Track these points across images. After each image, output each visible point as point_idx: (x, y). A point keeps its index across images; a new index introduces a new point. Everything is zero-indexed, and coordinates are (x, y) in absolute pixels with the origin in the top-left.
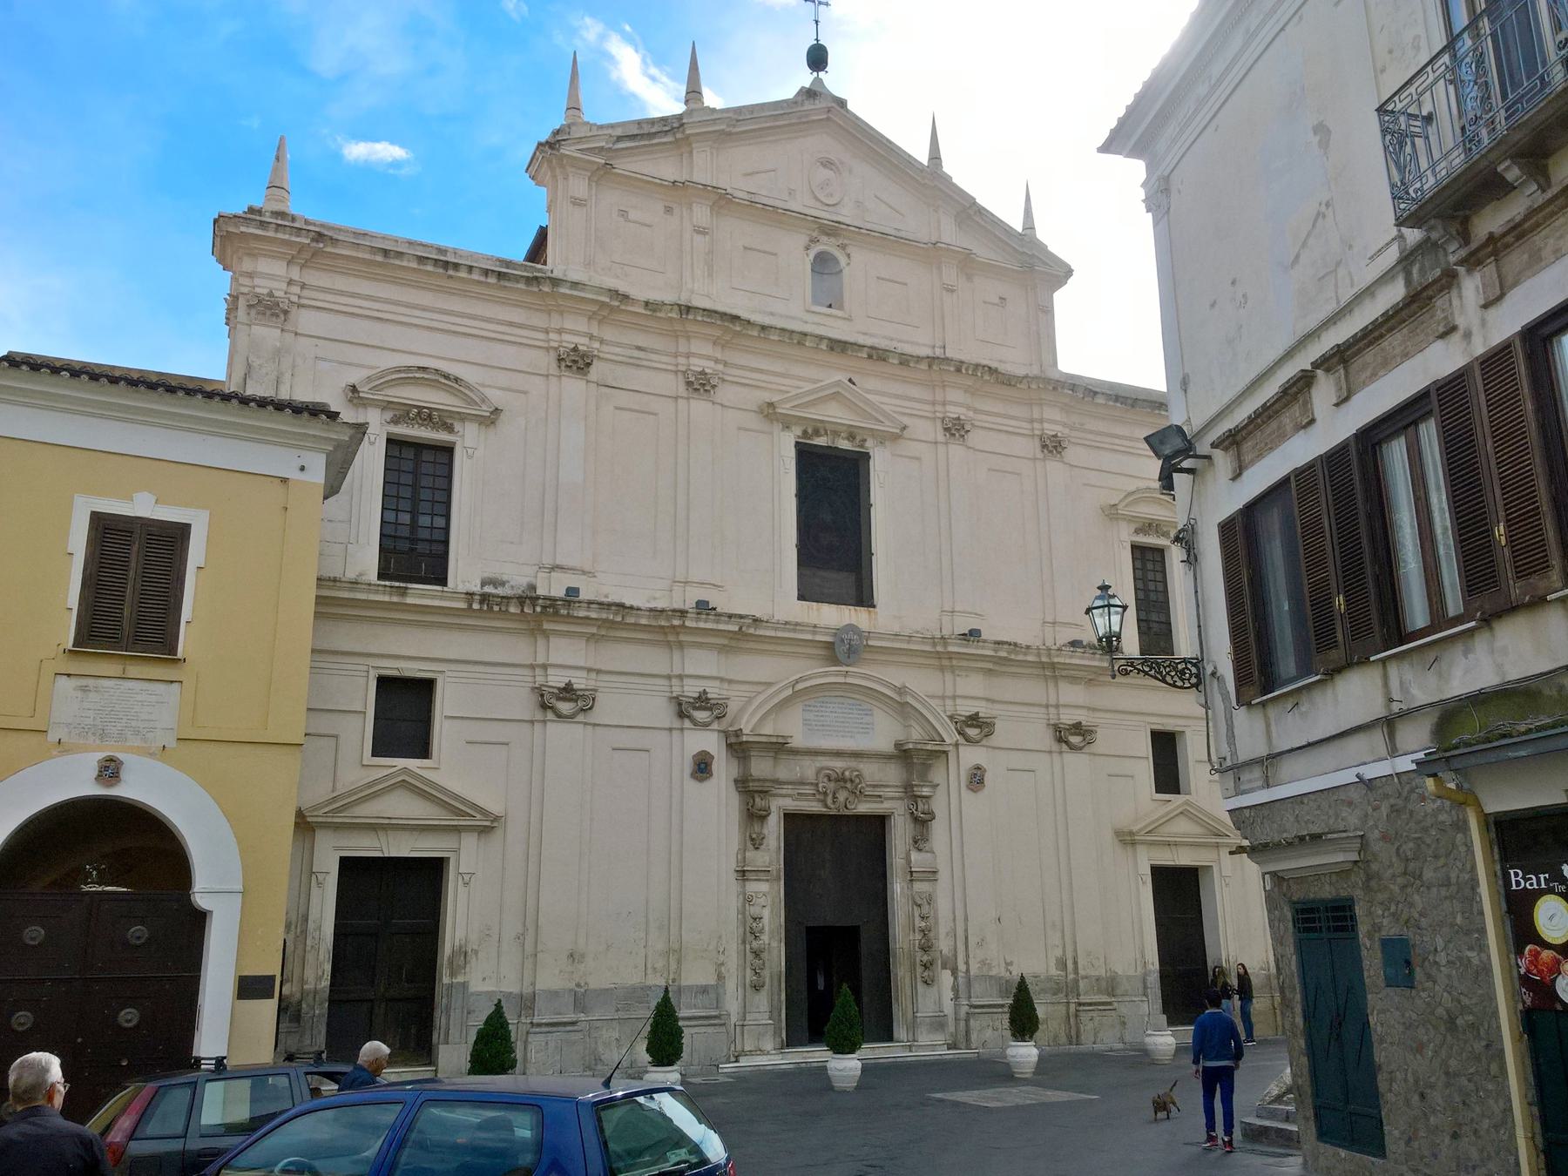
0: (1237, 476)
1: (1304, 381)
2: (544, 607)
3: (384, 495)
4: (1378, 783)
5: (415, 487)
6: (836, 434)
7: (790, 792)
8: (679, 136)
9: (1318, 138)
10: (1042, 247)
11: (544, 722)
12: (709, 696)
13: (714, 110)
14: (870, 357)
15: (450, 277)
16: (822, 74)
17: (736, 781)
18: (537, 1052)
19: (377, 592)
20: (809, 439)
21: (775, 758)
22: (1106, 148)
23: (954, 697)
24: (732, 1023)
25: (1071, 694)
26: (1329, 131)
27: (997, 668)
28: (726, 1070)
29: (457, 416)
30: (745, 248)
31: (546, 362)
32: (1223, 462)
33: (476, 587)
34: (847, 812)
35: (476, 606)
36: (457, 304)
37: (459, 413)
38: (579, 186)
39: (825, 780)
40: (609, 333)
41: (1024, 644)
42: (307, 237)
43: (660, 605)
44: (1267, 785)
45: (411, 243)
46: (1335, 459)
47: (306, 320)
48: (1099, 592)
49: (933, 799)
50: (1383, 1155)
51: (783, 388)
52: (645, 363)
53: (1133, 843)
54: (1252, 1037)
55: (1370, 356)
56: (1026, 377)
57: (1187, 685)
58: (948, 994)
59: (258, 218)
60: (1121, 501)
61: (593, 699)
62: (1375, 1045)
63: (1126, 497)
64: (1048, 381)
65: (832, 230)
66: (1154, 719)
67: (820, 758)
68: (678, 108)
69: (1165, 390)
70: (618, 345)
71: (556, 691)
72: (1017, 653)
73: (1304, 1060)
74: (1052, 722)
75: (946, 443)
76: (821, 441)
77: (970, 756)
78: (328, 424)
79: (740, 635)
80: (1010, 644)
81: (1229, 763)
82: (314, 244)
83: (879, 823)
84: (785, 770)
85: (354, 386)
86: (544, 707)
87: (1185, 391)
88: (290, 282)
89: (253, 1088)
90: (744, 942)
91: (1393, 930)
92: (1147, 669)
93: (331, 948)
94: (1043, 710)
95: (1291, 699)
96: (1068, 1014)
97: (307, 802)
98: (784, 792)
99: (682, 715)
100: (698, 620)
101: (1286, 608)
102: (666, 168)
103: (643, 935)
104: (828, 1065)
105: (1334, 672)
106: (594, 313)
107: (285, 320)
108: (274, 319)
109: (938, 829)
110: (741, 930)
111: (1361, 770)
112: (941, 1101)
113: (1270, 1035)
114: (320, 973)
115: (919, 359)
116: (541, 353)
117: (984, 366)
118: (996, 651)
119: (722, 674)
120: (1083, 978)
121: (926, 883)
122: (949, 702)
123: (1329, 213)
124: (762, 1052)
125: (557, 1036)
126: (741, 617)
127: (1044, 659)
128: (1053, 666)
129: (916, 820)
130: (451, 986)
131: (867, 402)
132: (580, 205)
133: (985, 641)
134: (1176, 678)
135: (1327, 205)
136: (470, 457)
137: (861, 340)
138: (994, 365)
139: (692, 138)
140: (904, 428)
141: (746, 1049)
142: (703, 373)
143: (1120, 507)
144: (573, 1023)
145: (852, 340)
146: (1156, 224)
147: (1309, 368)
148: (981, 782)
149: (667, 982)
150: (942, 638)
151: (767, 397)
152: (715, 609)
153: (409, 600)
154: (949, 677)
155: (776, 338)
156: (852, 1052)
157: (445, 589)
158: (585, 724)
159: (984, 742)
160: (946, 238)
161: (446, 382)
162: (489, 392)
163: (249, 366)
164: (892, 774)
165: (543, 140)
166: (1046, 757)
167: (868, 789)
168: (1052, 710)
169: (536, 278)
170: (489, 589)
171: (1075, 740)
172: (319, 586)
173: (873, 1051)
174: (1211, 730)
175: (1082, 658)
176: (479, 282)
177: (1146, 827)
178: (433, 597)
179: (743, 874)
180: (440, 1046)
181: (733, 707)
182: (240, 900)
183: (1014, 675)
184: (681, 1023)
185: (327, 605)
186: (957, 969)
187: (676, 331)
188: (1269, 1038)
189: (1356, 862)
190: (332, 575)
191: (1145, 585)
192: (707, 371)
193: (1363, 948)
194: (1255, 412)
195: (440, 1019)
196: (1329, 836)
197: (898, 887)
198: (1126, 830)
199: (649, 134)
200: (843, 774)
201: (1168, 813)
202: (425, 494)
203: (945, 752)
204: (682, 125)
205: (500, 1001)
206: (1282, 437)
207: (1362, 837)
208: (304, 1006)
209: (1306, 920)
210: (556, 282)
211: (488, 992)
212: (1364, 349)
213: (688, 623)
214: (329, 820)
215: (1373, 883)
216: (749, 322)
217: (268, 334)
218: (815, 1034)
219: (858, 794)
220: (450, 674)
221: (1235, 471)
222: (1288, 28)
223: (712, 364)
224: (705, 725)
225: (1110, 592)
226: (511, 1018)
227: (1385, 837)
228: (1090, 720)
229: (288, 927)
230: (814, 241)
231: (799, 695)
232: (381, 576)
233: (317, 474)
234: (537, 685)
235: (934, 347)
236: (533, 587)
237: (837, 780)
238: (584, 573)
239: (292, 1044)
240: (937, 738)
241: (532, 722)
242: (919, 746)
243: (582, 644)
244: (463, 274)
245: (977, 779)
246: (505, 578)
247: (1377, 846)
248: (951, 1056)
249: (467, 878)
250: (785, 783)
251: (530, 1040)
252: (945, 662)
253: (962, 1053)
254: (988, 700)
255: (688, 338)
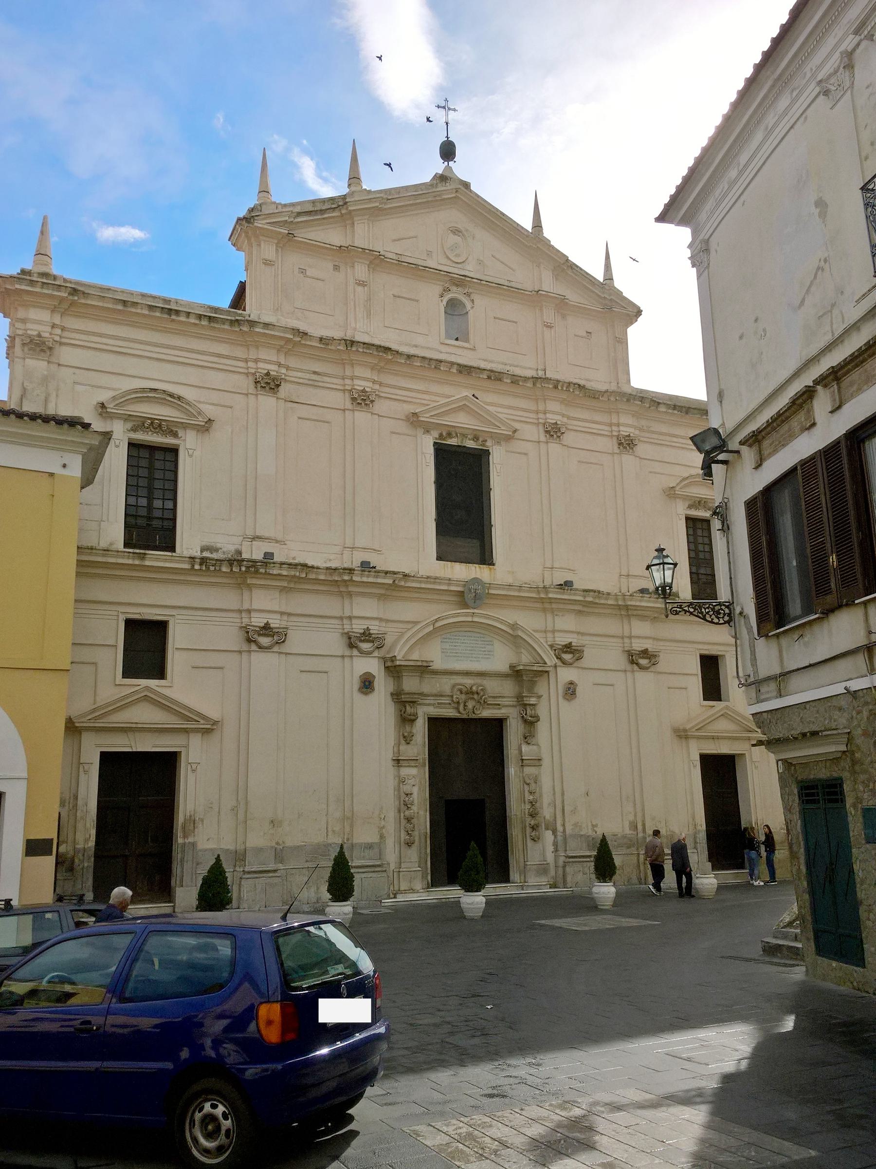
0: (758, 466)
1: (808, 394)
2: (248, 567)
3: (127, 485)
4: (860, 693)
5: (151, 479)
6: (464, 436)
7: (432, 702)
8: (343, 212)
9: (818, 210)
10: (619, 293)
11: (249, 652)
12: (371, 632)
13: (369, 192)
14: (489, 378)
15: (173, 320)
16: (451, 163)
17: (392, 694)
18: (247, 892)
19: (123, 557)
20: (444, 440)
21: (421, 677)
22: (662, 218)
23: (554, 631)
24: (391, 870)
25: (640, 628)
26: (826, 205)
27: (585, 609)
28: (386, 904)
29: (180, 425)
30: (394, 296)
31: (247, 384)
32: (748, 454)
33: (197, 553)
34: (474, 716)
35: (197, 567)
36: (178, 341)
37: (182, 423)
38: (268, 250)
39: (458, 693)
40: (293, 362)
41: (605, 591)
42: (65, 292)
43: (333, 565)
44: (780, 695)
45: (143, 295)
46: (830, 452)
47: (66, 355)
48: (656, 553)
49: (537, 707)
50: (864, 967)
51: (423, 402)
52: (320, 384)
53: (687, 738)
54: (775, 878)
55: (856, 375)
56: (607, 391)
57: (722, 621)
58: (550, 848)
59: (28, 278)
60: (678, 484)
61: (285, 635)
62: (858, 885)
63: (681, 481)
64: (623, 394)
65: (461, 281)
66: (700, 646)
67: (454, 677)
68: (344, 190)
69: (706, 399)
70: (301, 370)
71: (258, 629)
72: (599, 598)
73: (806, 897)
74: (626, 649)
75: (547, 443)
76: (453, 442)
77: (566, 675)
78: (82, 432)
79: (394, 586)
80: (595, 592)
81: (752, 679)
82: (71, 297)
83: (499, 724)
84: (429, 686)
85: (103, 404)
86: (249, 641)
87: (721, 402)
88: (54, 326)
89: (34, 921)
90: (399, 811)
91: (871, 801)
92: (692, 610)
93: (95, 818)
94: (620, 640)
95: (797, 632)
96: (639, 863)
97: (74, 713)
98: (427, 702)
99: (351, 646)
100: (362, 575)
101: (795, 564)
102: (335, 237)
103: (325, 806)
104: (461, 900)
105: (828, 612)
106: (282, 347)
107: (50, 355)
108: (42, 354)
109: (542, 728)
110: (397, 803)
111: (848, 684)
112: (542, 926)
113: (788, 876)
114: (88, 836)
115: (526, 379)
116: (242, 377)
117: (575, 384)
118: (585, 597)
119: (381, 616)
120: (248, 390)
121: (533, 768)
122: (550, 635)
123: (827, 267)
124: (412, 891)
125: (262, 881)
126: (394, 573)
127: (620, 603)
128: (627, 608)
129: (525, 721)
130: (184, 844)
131: (487, 412)
132: (268, 264)
133: (577, 590)
134: (713, 616)
135: (825, 261)
136: (191, 456)
137: (483, 365)
138: (582, 383)
139: (353, 213)
140: (515, 431)
141: (402, 888)
142: (364, 391)
143: (677, 489)
144: (275, 871)
145: (475, 365)
146: (699, 276)
147: (811, 384)
148: (574, 693)
149: (343, 841)
150: (544, 587)
151: (412, 408)
152: (375, 568)
153: (147, 563)
154: (549, 617)
155: (419, 364)
156: (478, 890)
157: (174, 554)
158: (280, 653)
159: (576, 664)
160: (546, 287)
161: (172, 400)
162: (201, 406)
163: (24, 390)
164: (508, 688)
165: (241, 216)
166: (622, 674)
167: (489, 699)
168: (627, 640)
169: (237, 320)
170: (206, 554)
171: (643, 662)
172: (79, 553)
173: (494, 890)
174: (739, 653)
175: (649, 602)
176: (195, 324)
177: (697, 725)
178: (166, 560)
179: (398, 762)
180: (177, 888)
181: (389, 640)
182: (25, 786)
183: (599, 614)
184: (352, 871)
185: (93, 567)
186: (556, 829)
187: (343, 360)
188: (787, 879)
189: (844, 752)
190: (89, 545)
191: (696, 547)
192: (367, 389)
193: (849, 815)
194: (771, 418)
195: (176, 868)
196: (824, 733)
197: (512, 771)
198: (681, 728)
199: (321, 210)
200: (471, 688)
201: (713, 715)
202: (158, 484)
203: (547, 672)
204: (346, 203)
205: (219, 856)
206: (792, 436)
207: (849, 733)
208: (76, 861)
209: (807, 795)
210: (252, 323)
211: (211, 850)
212: (852, 370)
213: (355, 578)
214: (92, 725)
215: (857, 768)
216: (397, 352)
217: (38, 365)
218: (451, 880)
219: (484, 704)
220: (180, 617)
221: (757, 462)
222: (796, 127)
223: (370, 384)
224: (368, 654)
225: (665, 553)
226: (228, 867)
227: (865, 734)
228: (655, 647)
229: (62, 803)
230: (447, 290)
231: (438, 631)
232: (126, 545)
233: (75, 470)
234: (243, 625)
235: (537, 370)
236: (239, 553)
237: (467, 693)
238: (277, 542)
239: (68, 888)
240: (541, 661)
241: (240, 652)
242: (528, 668)
243: (277, 594)
244: (182, 318)
245: (570, 691)
246: (219, 545)
247: (859, 741)
248: (553, 893)
249: (194, 766)
250: (428, 696)
251: (242, 883)
252: (547, 606)
253: (561, 891)
254: (578, 633)
255: (352, 365)
